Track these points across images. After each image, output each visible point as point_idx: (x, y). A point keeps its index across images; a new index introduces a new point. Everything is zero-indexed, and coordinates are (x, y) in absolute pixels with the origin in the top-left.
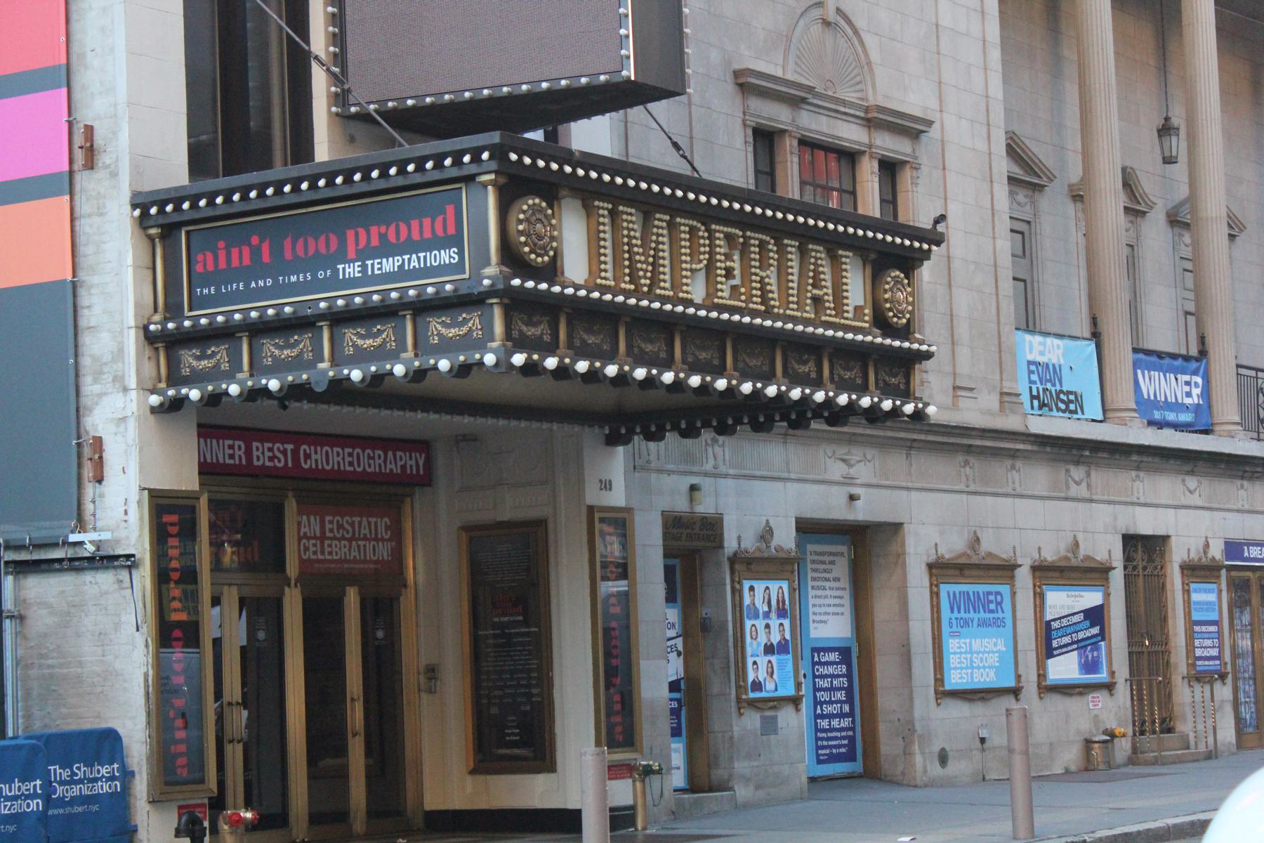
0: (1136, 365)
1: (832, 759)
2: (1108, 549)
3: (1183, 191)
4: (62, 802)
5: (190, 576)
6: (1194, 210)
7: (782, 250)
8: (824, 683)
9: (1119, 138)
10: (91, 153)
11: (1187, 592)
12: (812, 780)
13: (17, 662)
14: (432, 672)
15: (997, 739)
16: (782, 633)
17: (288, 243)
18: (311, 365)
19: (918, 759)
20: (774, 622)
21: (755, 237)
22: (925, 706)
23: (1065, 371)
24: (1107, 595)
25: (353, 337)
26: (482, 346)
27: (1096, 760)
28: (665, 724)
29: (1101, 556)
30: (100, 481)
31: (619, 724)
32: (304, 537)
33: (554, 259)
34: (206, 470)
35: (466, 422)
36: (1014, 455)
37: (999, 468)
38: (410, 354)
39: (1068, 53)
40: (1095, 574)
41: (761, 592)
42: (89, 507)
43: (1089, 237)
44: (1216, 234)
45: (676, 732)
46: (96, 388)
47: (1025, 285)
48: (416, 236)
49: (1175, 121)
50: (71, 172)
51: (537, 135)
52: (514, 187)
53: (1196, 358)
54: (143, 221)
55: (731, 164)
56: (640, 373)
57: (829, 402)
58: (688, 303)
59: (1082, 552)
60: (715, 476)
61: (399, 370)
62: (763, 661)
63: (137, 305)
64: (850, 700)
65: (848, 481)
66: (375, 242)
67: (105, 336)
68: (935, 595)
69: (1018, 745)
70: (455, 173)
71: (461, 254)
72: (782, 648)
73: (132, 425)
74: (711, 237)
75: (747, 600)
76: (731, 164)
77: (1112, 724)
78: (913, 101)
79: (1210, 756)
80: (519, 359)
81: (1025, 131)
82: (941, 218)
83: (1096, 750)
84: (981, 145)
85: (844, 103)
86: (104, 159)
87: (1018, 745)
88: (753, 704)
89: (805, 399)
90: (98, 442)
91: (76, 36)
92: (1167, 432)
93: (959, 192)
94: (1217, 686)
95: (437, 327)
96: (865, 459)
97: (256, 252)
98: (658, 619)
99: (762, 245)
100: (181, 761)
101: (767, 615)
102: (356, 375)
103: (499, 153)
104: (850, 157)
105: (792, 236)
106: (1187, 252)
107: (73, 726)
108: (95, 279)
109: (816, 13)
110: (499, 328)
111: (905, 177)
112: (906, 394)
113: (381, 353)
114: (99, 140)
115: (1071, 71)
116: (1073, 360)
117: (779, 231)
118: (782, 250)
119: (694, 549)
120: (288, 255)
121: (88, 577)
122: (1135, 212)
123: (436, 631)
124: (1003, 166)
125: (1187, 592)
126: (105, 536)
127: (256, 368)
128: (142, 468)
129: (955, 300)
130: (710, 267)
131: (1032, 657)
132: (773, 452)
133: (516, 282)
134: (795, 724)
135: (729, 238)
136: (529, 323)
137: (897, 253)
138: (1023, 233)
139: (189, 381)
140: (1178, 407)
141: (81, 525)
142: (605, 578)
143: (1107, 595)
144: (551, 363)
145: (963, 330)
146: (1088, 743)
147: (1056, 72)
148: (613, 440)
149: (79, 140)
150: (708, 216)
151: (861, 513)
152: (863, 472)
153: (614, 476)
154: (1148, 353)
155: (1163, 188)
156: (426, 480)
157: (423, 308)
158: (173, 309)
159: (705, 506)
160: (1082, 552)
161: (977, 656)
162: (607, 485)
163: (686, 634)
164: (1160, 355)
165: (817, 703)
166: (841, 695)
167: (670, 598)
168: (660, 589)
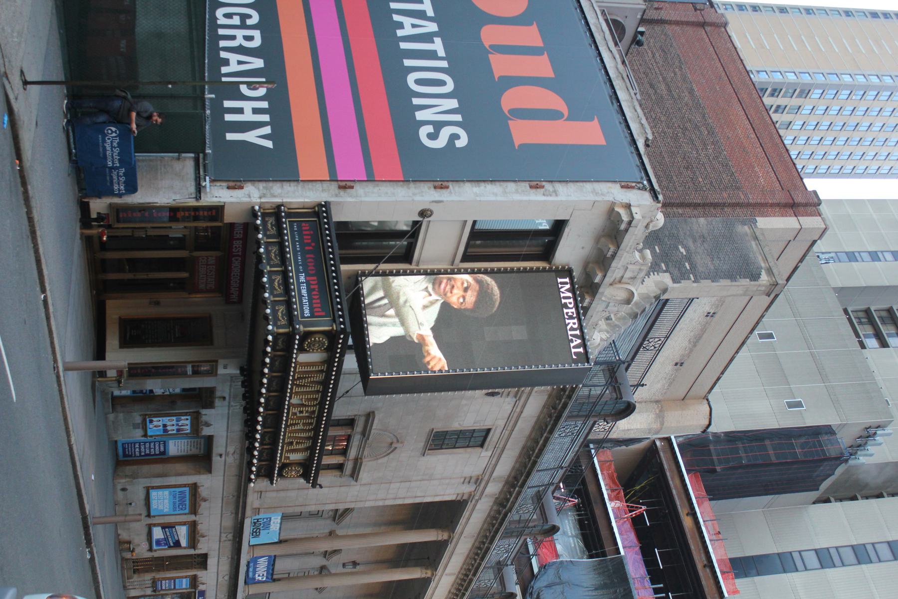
0: (270, 557)
1: (124, 449)
2: (202, 548)
3: (333, 571)
4: (111, 172)
5: (196, 218)
6: (326, 575)
7: (309, 430)
8: (152, 446)
9: (351, 548)
10: (343, 188)
11: (186, 577)
12: (116, 442)
13: (162, 157)
14: (157, 303)
15: (131, 510)
16: (171, 431)
17: (312, 256)
18: (268, 264)
19: (124, 481)
20: (175, 428)
21: (314, 421)
22: (143, 482)
23: (267, 531)
24: (185, 548)
25: (278, 279)
26: (274, 325)
27: (123, 546)
28: (137, 388)
29: (200, 546)
30: (228, 188)
31: (137, 371)
32: (208, 258)
33: (306, 350)
34: (232, 225)
35: (248, 317)
36: (237, 513)
37: (232, 508)
38: (272, 299)
39: (383, 528)
40: (193, 543)
41: (186, 423)
42: (218, 184)
43: (317, 538)
44: (318, 584)
45: (134, 392)
46: (261, 188)
47: (299, 516)
48: (314, 301)
49: (358, 567)
50: (337, 181)
51: (350, 342)
52: (332, 336)
53: (272, 578)
54: (320, 205)
55: (340, 411)
56: (265, 381)
57: (255, 448)
58: (290, 397)
59: (201, 539)
60: (229, 407)
61: (267, 295)
62: (160, 423)
63: (290, 203)
64: (146, 455)
65: (227, 454)
66: (312, 287)
67: (279, 191)
68: (185, 486)
69: (128, 518)
70: (336, 316)
71: (308, 317)
72: (165, 431)
73: (246, 200)
74: (314, 406)
75: (183, 418)
76: (340, 411)
77: (137, 551)
78: (364, 475)
79: (125, 587)
80: (270, 338)
81: (354, 514)
82: (321, 487)
83: (127, 546)
84: (349, 499)
85: (363, 450)
86: (342, 192)
87: (128, 518)
88: (144, 420)
89: (256, 440)
90: (242, 188)
91: (385, 184)
92: (245, 568)
93: (332, 491)
94: (151, 589)
95: (281, 309)
96: (235, 460)
97: (309, 245)
98: (176, 386)
99: (311, 424)
100: (125, 215)
101: (177, 425)
102: (265, 280)
103: (343, 331)
104: (344, 452)
105: (315, 434)
106: (311, 573)
107: (139, 176)
108: (300, 188)
109: (395, 440)
110: (281, 331)
111: (337, 473)
112: (258, 476)
113: (272, 289)
114: (349, 190)
115: (377, 530)
116: (268, 536)
117: (316, 430)
118: (309, 430)
119: (203, 399)
120: (307, 256)
121: (193, 183)
122: (325, 554)
123: (172, 305)
124: (341, 507)
125: (186, 577)
126: (208, 190)
127: (268, 244)
128: (232, 203)
129: (292, 491)
130: (303, 405)
131: (162, 521)
132: (237, 427)
133: (298, 337)
134: (138, 434)
135: (314, 412)
136: (283, 341)
137: (309, 471)
138: (317, 515)
139: (263, 221)
140: (255, 572)
141: (212, 181)
142: (193, 367)
143: (185, 548)
144: (269, 349)
145: (282, 494)
146: (129, 542)
147: (377, 524)
148: (242, 369)
149: (349, 184)
150: (322, 404)
151: (215, 459)
152: (230, 459)
153: (228, 370)
154: (274, 561)
155: (334, 564)
156: (228, 301)
157: (289, 304)
158: (289, 215)
159: (218, 403)
160: (201, 539)
161: (162, 501)
162: (225, 367)
163: (171, 395)
164: (274, 565)
165: (145, 443)
166: (148, 452)
167: (184, 390)
168: (187, 386)
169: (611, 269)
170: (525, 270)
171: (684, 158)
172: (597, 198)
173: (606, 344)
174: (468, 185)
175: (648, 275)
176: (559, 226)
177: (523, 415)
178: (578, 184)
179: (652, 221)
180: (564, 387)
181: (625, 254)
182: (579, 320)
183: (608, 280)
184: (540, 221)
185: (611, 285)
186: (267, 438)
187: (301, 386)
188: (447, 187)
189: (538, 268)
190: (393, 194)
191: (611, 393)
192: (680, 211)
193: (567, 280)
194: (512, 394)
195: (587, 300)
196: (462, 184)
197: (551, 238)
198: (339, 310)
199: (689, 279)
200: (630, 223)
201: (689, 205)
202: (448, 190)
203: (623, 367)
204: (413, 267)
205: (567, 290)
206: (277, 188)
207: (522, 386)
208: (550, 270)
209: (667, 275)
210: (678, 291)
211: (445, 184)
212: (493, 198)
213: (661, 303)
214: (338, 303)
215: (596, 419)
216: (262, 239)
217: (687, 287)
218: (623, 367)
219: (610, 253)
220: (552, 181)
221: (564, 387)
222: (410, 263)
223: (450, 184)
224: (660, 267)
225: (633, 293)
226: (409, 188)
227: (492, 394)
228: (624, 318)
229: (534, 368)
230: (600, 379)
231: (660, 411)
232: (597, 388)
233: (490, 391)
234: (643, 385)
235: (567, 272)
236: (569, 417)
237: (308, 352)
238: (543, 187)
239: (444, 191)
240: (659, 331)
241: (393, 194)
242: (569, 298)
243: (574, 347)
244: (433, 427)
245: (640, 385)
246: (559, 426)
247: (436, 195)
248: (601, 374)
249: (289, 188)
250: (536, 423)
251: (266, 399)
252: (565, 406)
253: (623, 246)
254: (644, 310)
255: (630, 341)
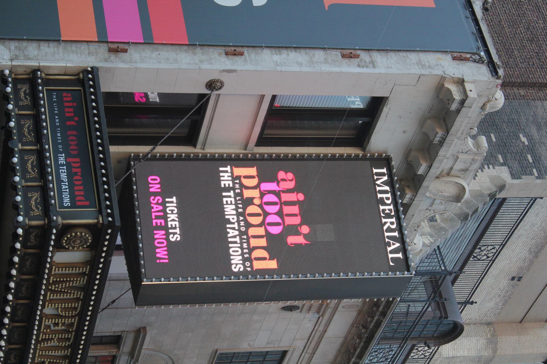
7: (66, 348)
10: (115, 51)
18: (20, 141)
21: (72, 336)
25: (32, 159)
33: (64, 248)
38: (24, 184)
46: (13, 48)
50: (107, 42)
51: (119, 241)
54: (85, 71)
55: (105, 326)
58: (43, 306)
61: (17, 179)
63: (49, 67)
66: (74, 170)
67: (36, 52)
70: (103, 206)
71: (68, 207)
74: (72, 317)
76: (105, 326)
80: (20, 231)
86: (113, 56)
91: (165, 48)
95: (35, 196)
99: (68, 339)
102: (15, 160)
103: (111, 225)
108: (61, 50)
110: (34, 223)
114: (121, 55)
117: (74, 347)
118: (66, 348)
120: (69, 133)
127: (19, 117)
130: (59, 316)
133: (54, 231)
135: (72, 324)
136: (36, 236)
139: (14, 88)
144: (18, 246)
149: (121, 46)
150: (82, 316)
157: (44, 191)
158: (47, 82)
169: (438, 158)
170: (333, 158)
171: (528, 29)
172: (424, 72)
173: (429, 250)
174: (267, 51)
175: (482, 168)
176: (376, 105)
177: (327, 335)
178: (401, 54)
179: (489, 101)
180: (379, 300)
181: (456, 140)
182: (399, 219)
183: (434, 171)
184: (353, 99)
185: (437, 177)
186: (12, 357)
187: (57, 292)
188: (242, 54)
189: (349, 156)
190: (176, 60)
191: (433, 311)
192: (522, 92)
193: (384, 170)
194: (314, 309)
195: (408, 196)
196: (259, 50)
197: (366, 119)
198: (107, 199)
199: (532, 174)
200: (462, 103)
201: (532, 85)
202: (243, 57)
203: (450, 278)
204: (197, 150)
205: (385, 183)
206: (32, 49)
207: (327, 298)
208: (364, 158)
209: (505, 169)
210: (518, 188)
211: (239, 49)
212: (296, 69)
213: (497, 202)
214: (105, 191)
215: (415, 342)
216: (13, 110)
217: (529, 184)
218: (450, 278)
219: (437, 139)
220: (369, 50)
221: (379, 300)
222: (195, 146)
223: (245, 50)
224: (496, 158)
225: (464, 188)
226: (195, 54)
227: (290, 309)
228: (452, 220)
229: (342, 276)
230: (422, 293)
231: (493, 335)
232: (417, 304)
233: (289, 303)
234: (472, 303)
235: (385, 161)
236: (384, 338)
237: (67, 250)
238: (357, 56)
239: (237, 58)
240: (493, 237)
241: (176, 60)
242: (385, 192)
243: (392, 252)
244: (216, 348)
245: (469, 302)
246: (370, 349)
247: (227, 63)
248: (422, 288)
249: (47, 49)
250: (342, 345)
251: (13, 308)
252: (378, 325)
253: (454, 129)
254: (476, 210)
255: (458, 248)
